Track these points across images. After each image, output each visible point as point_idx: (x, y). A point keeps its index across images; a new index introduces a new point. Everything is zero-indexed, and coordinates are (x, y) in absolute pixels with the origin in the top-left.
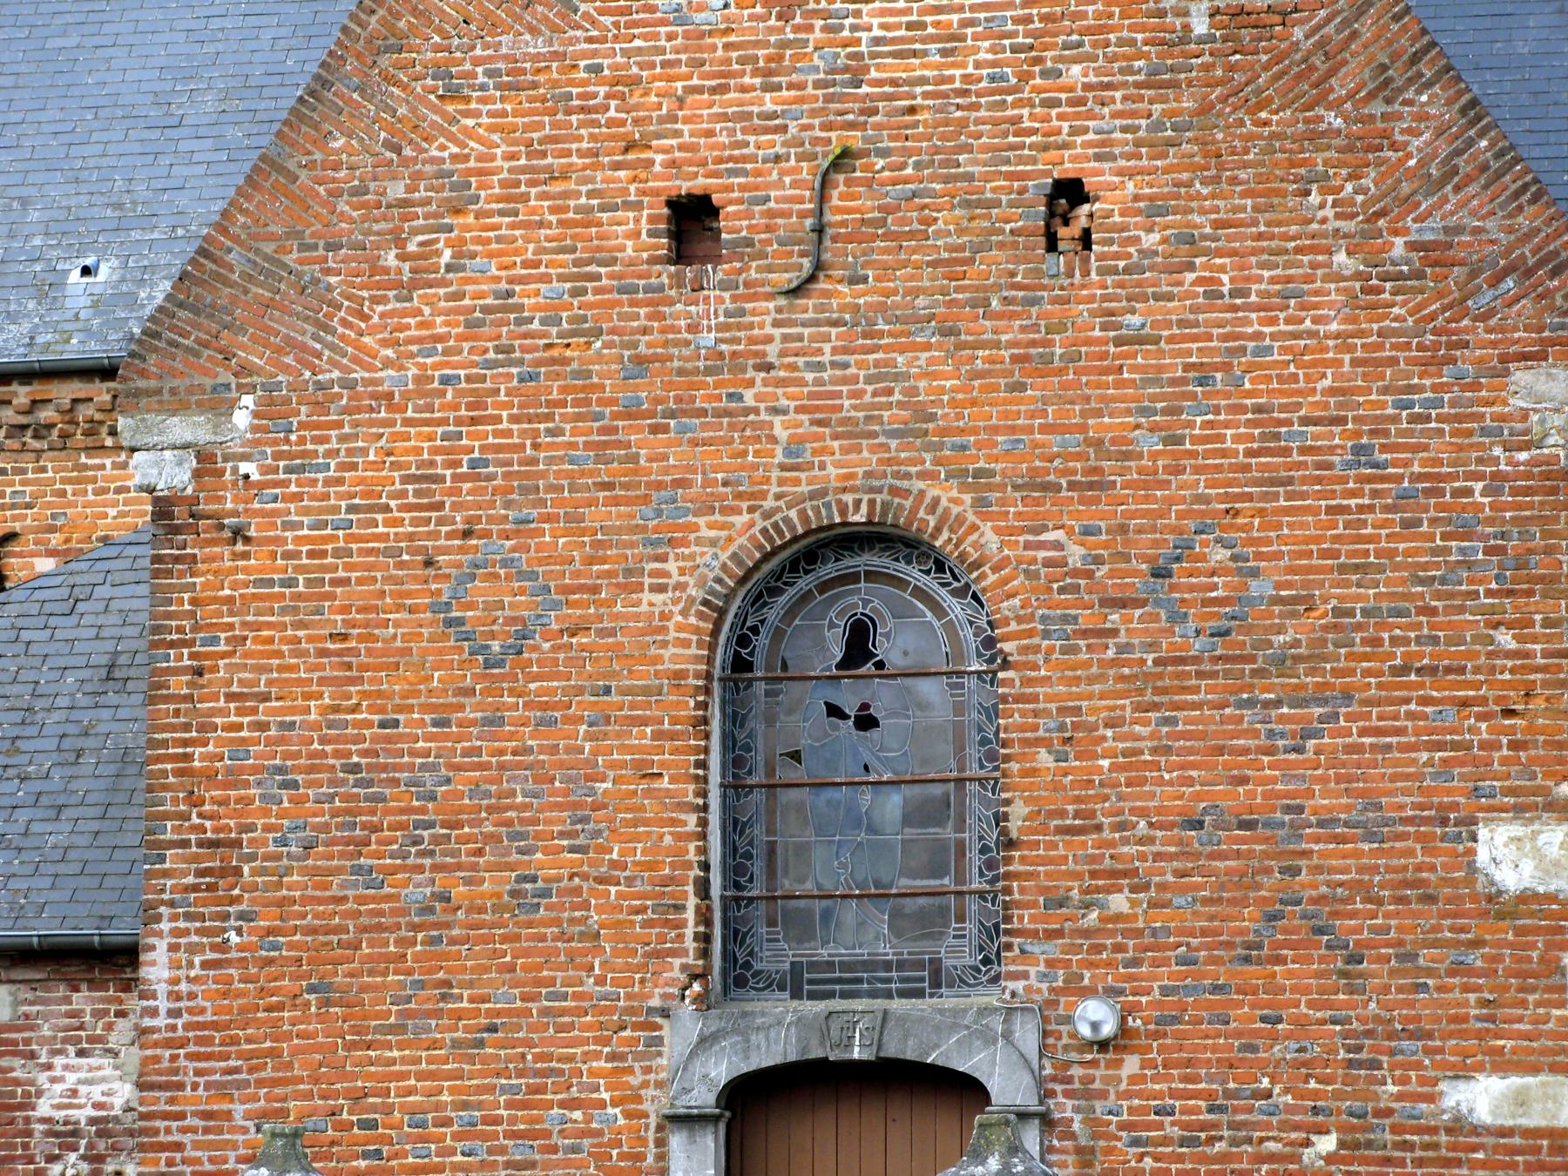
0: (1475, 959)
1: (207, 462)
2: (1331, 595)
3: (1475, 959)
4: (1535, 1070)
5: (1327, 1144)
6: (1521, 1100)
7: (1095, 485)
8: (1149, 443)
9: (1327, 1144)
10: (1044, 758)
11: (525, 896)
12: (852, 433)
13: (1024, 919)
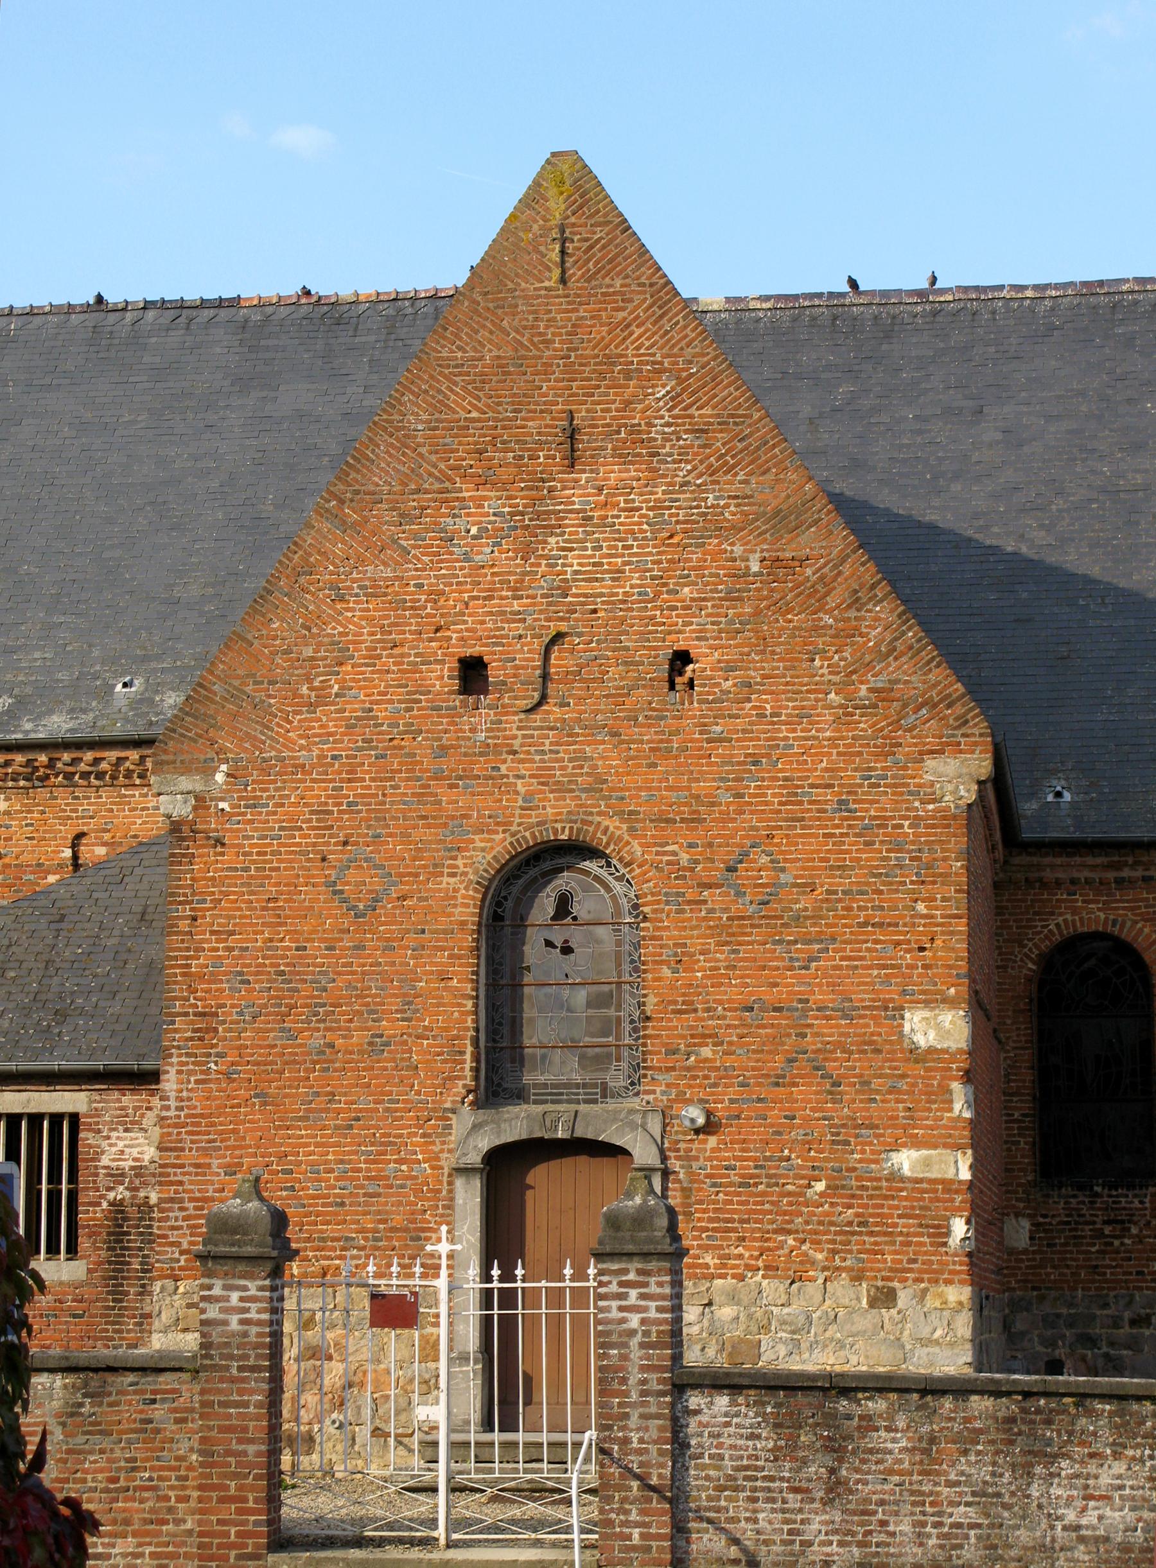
0: (903, 1085)
1: (201, 802)
2: (825, 882)
3: (903, 1085)
4: (935, 1147)
5: (820, 1186)
6: (927, 1163)
7: (695, 820)
8: (726, 798)
9: (820, 1186)
10: (666, 972)
11: (376, 1045)
12: (561, 789)
13: (654, 1061)
